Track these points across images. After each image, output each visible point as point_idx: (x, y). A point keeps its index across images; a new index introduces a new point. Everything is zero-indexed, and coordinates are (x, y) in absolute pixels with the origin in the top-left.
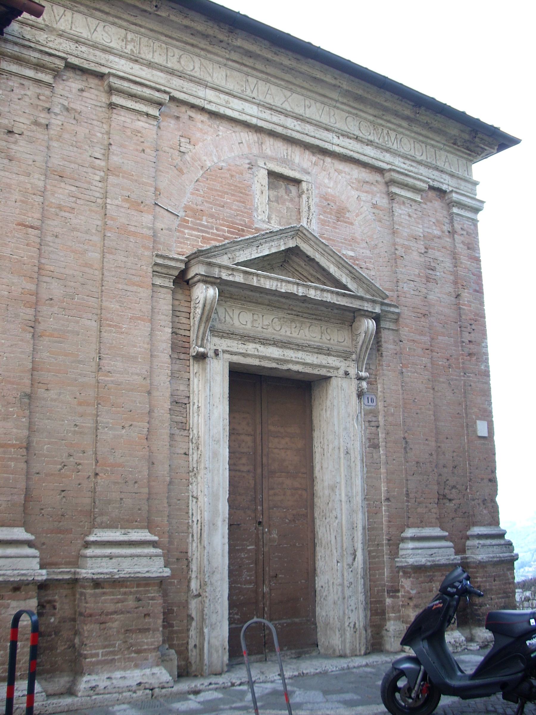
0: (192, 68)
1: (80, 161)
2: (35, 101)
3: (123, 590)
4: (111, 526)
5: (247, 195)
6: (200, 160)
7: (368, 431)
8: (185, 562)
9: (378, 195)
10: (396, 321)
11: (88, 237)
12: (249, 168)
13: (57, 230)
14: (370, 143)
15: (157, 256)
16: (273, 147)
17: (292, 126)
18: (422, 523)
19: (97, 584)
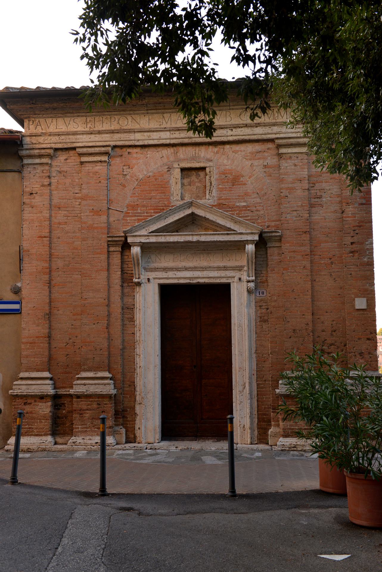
0: (126, 123)
1: (68, 197)
2: (42, 174)
3: (91, 400)
5: (166, 188)
6: (135, 176)
9: (269, 158)
10: (280, 240)
11: (74, 235)
12: (168, 171)
13: (59, 235)
15: (108, 237)
16: (183, 152)
19: (78, 397)
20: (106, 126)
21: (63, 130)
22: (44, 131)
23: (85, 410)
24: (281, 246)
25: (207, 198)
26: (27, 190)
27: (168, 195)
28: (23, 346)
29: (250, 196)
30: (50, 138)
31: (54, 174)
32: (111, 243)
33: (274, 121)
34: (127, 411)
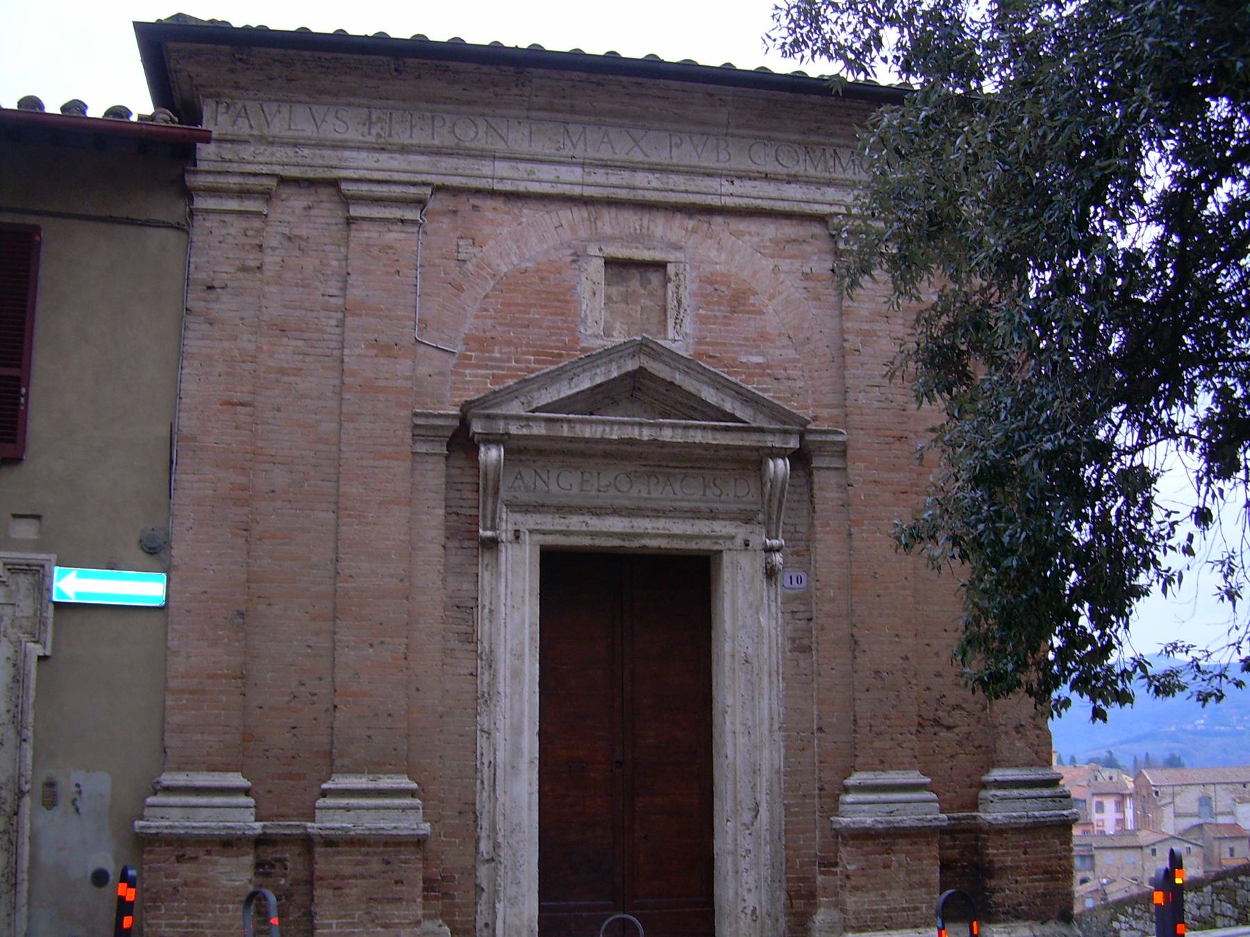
4: (356, 770)
6: (489, 265)
7: (790, 627)
8: (471, 816)
9: (815, 258)
12: (574, 261)
14: (792, 179)
16: (609, 221)
17: (645, 184)
18: (883, 764)
19: (330, 842)
20: (420, 137)
21: (308, 133)
22: (255, 133)
23: (349, 878)
24: (845, 469)
25: (670, 336)
26: (202, 276)
27: (573, 322)
28: (170, 701)
29: (772, 341)
30: (270, 150)
31: (274, 243)
32: (422, 432)
33: (827, 175)
34: (452, 879)
